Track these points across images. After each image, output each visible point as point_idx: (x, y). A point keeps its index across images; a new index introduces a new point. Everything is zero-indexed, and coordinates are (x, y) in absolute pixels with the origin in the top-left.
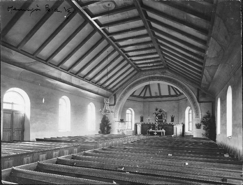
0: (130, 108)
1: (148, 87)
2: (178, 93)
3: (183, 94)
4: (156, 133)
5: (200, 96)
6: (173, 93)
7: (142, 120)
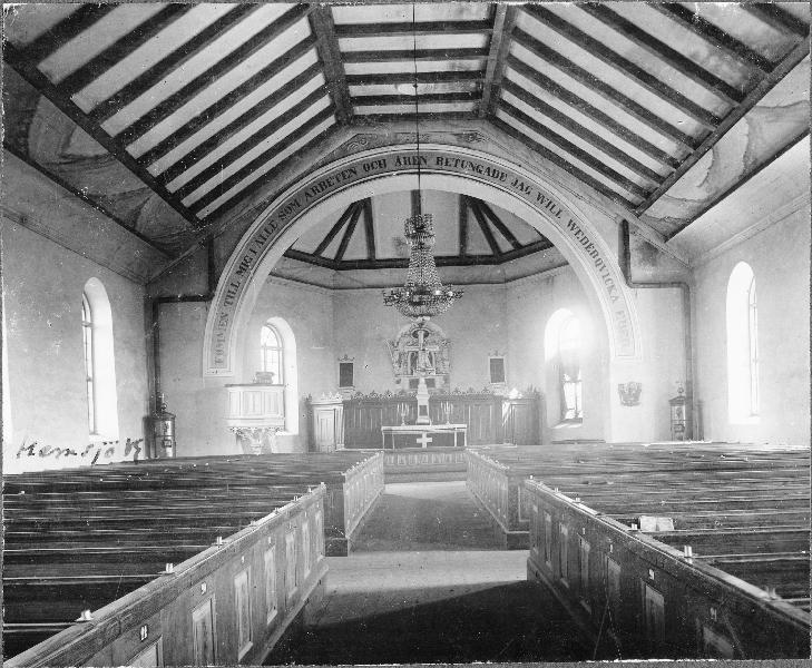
0: (273, 320)
1: (362, 208)
2: (506, 246)
3: (544, 244)
4: (430, 440)
5: (635, 257)
6: (477, 246)
7: (346, 372)
